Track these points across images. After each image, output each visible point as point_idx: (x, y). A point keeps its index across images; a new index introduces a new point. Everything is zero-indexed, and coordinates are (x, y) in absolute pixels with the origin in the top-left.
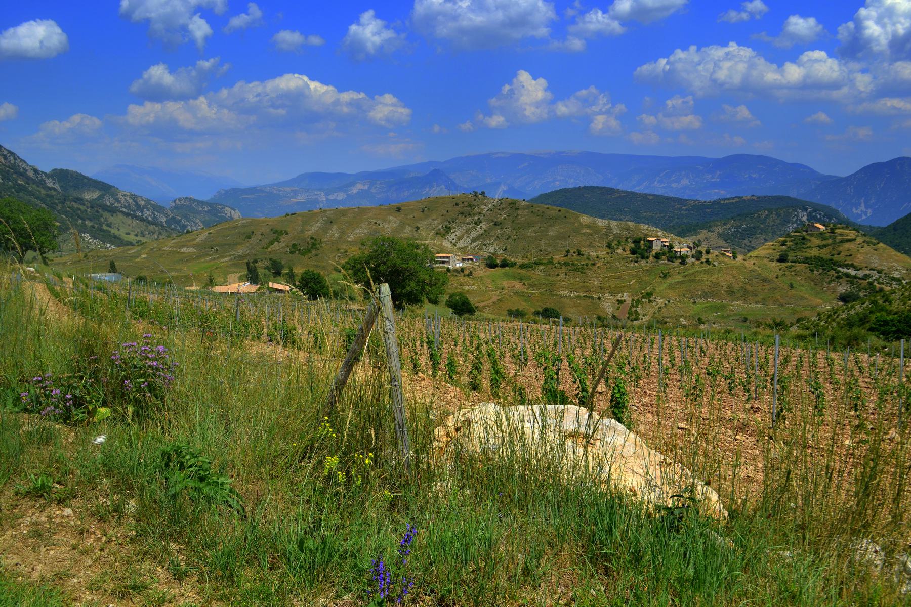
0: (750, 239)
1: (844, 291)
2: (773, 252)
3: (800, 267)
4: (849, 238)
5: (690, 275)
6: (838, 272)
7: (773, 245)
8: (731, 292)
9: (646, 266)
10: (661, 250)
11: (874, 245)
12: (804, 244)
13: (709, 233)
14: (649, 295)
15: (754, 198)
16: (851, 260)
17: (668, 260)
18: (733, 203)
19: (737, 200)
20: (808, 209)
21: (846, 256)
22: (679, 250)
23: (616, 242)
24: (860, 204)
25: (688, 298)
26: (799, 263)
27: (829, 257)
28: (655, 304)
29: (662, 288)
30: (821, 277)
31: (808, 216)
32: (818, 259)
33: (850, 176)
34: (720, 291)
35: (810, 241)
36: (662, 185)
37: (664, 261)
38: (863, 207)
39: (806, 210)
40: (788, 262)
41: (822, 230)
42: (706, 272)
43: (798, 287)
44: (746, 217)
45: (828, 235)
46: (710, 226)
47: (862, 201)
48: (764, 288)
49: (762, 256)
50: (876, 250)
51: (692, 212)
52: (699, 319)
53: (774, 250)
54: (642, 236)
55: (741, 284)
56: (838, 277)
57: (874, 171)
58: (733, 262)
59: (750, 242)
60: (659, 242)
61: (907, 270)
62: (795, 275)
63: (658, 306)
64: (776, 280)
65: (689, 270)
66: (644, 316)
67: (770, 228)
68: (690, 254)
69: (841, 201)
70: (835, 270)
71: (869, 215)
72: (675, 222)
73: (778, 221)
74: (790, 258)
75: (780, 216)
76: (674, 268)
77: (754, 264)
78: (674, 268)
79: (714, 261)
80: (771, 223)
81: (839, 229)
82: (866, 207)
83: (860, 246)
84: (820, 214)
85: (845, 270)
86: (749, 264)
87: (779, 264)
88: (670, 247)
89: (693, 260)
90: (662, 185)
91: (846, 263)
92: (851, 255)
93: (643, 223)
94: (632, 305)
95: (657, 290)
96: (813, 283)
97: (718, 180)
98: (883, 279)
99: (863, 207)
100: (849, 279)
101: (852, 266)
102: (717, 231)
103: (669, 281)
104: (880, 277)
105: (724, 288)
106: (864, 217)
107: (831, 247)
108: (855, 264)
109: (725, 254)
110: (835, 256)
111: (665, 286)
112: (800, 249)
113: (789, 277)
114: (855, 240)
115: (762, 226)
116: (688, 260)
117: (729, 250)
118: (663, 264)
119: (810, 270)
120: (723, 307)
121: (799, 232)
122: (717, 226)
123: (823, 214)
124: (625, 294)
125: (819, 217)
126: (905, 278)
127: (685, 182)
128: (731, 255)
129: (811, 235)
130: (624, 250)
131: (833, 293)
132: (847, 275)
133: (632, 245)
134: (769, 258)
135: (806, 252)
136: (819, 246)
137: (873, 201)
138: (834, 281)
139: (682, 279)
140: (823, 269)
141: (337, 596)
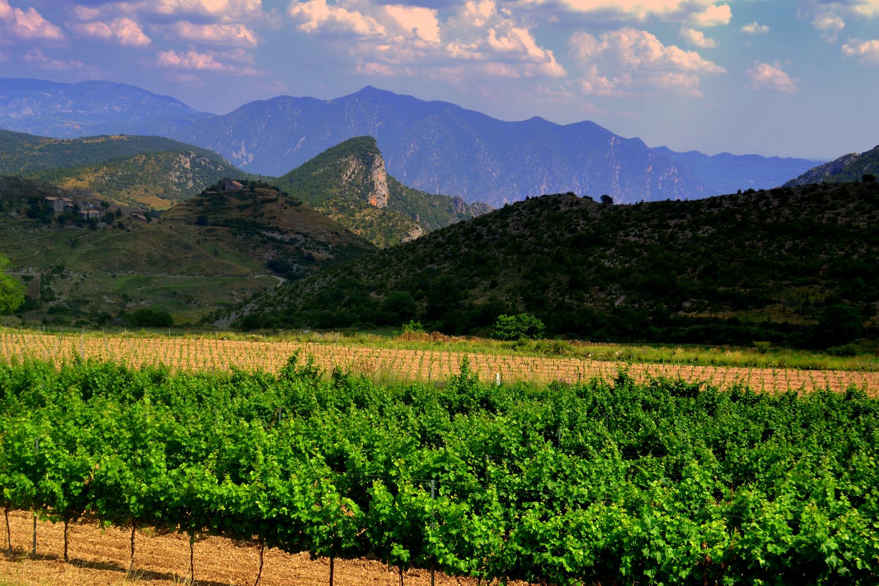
0: (129, 190)
1: (271, 258)
2: (189, 213)
6: (263, 236)
8: (152, 262)
9: (48, 232)
10: (64, 213)
12: (222, 204)
14: (60, 269)
15: (124, 137)
18: (98, 143)
19: (104, 139)
20: (191, 154)
22: (86, 212)
23: (7, 203)
24: (240, 149)
26: (220, 226)
27: (251, 219)
28: (69, 279)
33: (229, 115)
35: (229, 201)
38: (243, 151)
39: (188, 155)
40: (207, 225)
44: (120, 162)
46: (78, 173)
47: (242, 144)
48: (186, 255)
49: (178, 218)
52: (125, 296)
53: (190, 211)
56: (264, 242)
57: (255, 109)
58: (148, 226)
59: (129, 193)
61: (332, 233)
62: (218, 240)
63: (74, 282)
66: (60, 295)
67: (150, 177)
68: (98, 217)
70: (259, 233)
71: (250, 161)
72: (26, 165)
73: (158, 169)
74: (209, 220)
75: (160, 161)
77: (170, 227)
78: (83, 235)
80: (151, 171)
82: (247, 152)
84: (205, 161)
85: (270, 234)
87: (197, 227)
89: (104, 224)
91: (270, 226)
94: (43, 283)
96: (237, 249)
97: (70, 111)
98: (309, 244)
99: (243, 151)
100: (275, 244)
101: (277, 229)
104: (307, 241)
105: (144, 258)
106: (245, 163)
114: (276, 200)
115: (141, 174)
120: (147, 281)
121: (215, 190)
122: (86, 173)
123: (208, 160)
124: (31, 269)
125: (203, 163)
126: (331, 241)
127: (28, 111)
130: (19, 212)
131: (259, 259)
132: (273, 240)
133: (29, 206)
135: (225, 213)
136: (239, 207)
138: (259, 246)
140: (247, 233)
141: (796, 456)
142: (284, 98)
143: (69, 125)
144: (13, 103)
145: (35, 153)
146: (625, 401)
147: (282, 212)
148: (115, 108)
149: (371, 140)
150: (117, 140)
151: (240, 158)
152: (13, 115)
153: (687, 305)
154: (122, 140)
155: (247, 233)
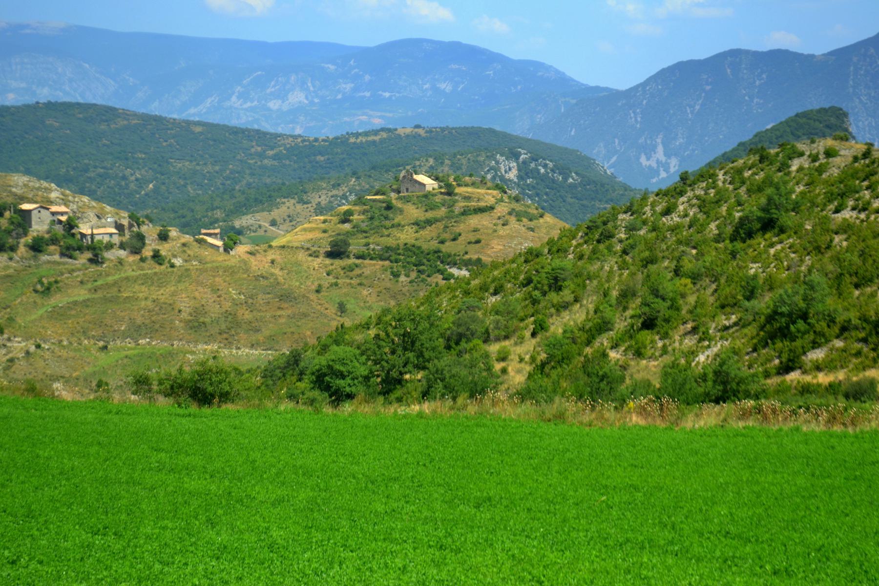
3: (371, 267)
4: (482, 204)
5: (108, 286)
7: (325, 222)
10: (48, 232)
11: (531, 220)
12: (386, 218)
13: (299, 207)
15: (421, 131)
16: (476, 253)
17: (62, 255)
18: (374, 142)
19: (384, 135)
20: (520, 154)
21: (469, 243)
22: (89, 232)
24: (654, 149)
25: (93, 337)
26: (371, 259)
27: (434, 244)
29: (33, 317)
30: (412, 289)
31: (519, 170)
32: (410, 249)
33: (635, 89)
34: (172, 322)
35: (401, 211)
36: (249, 104)
37: (51, 255)
39: (516, 156)
40: (348, 257)
41: (429, 188)
42: (147, 280)
43: (358, 311)
45: (438, 199)
47: (659, 140)
49: (295, 244)
50: (532, 230)
51: (287, 162)
53: (325, 231)
54: (10, 200)
55: (227, 305)
60: (45, 214)
62: (360, 284)
64: (313, 296)
65: (107, 275)
69: (617, 141)
72: (244, 182)
75: (459, 168)
76: (71, 272)
77: (273, 262)
78: (71, 272)
79: (175, 256)
81: (466, 185)
82: (668, 155)
83: (501, 222)
84: (545, 166)
86: (259, 264)
87: (328, 261)
88: (70, 226)
89: (122, 253)
90: (249, 104)
91: (467, 257)
92: (478, 242)
93: (17, 171)
95: (20, 321)
102: (317, 200)
103: (58, 300)
107: (441, 226)
108: (483, 258)
109: (205, 241)
110: (447, 244)
111: (41, 312)
112: (377, 230)
113: (344, 290)
114: (492, 208)
116: (108, 255)
117: (217, 231)
118: (49, 262)
119: (392, 273)
121: (383, 194)
122: (318, 189)
123: (551, 165)
125: (542, 171)
127: (297, 97)
128: (219, 243)
129: (407, 200)
134: (308, 249)
135: (388, 236)
136: (416, 224)
137: (680, 141)
139: (88, 296)
140: (419, 271)
142: (735, 53)
143: (364, 118)
144: (273, 83)
145: (266, 161)
146: (301, 575)
147: (495, 231)
148: (443, 86)
149: (848, 114)
150: (407, 136)
151: (654, 165)
152: (274, 105)
153: (818, 355)
154: (416, 136)
155: (419, 271)
